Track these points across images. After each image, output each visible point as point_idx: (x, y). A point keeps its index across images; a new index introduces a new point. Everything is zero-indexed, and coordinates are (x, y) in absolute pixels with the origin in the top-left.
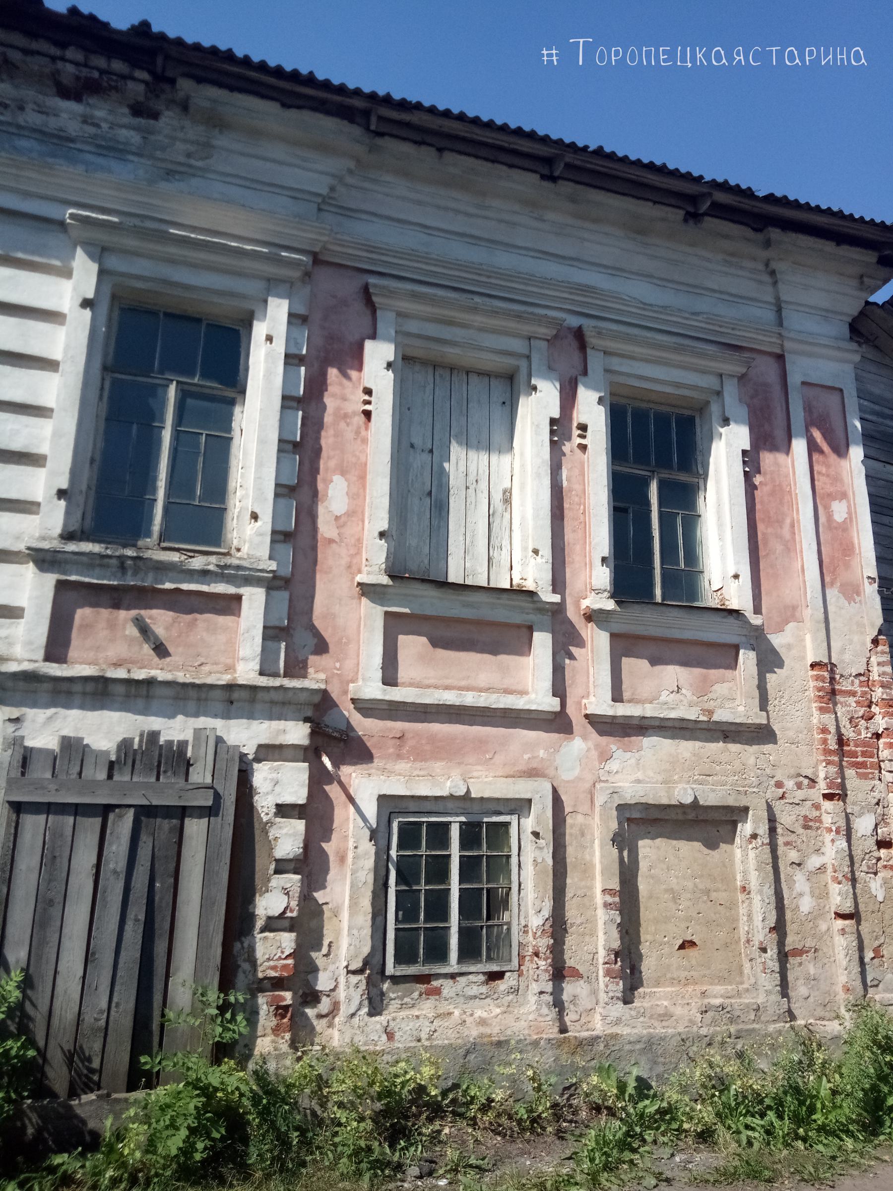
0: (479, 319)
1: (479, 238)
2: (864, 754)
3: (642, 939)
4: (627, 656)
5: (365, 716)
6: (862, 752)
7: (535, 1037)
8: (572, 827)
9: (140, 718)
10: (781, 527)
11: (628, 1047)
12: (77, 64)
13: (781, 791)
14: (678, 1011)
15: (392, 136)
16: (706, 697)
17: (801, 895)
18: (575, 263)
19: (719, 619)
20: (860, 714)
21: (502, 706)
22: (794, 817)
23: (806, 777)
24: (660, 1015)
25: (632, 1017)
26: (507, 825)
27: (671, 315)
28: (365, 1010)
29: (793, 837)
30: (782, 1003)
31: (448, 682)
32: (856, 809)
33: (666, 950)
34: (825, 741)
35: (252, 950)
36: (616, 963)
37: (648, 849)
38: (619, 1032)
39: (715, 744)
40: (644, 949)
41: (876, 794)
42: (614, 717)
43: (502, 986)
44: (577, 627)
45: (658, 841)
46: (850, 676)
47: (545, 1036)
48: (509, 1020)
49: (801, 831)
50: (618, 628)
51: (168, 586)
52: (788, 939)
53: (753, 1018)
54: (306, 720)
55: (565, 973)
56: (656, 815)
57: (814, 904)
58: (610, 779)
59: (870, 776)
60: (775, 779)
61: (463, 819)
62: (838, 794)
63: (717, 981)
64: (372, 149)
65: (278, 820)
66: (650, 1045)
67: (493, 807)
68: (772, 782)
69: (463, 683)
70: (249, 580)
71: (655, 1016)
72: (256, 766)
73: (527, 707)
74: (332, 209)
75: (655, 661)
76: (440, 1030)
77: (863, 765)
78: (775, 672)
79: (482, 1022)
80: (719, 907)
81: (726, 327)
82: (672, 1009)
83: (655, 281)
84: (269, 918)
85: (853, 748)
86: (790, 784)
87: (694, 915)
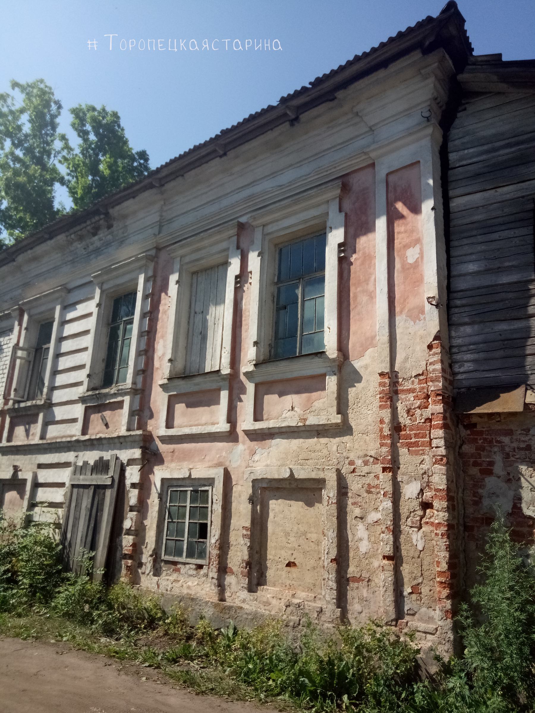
0: (206, 242)
1: (214, 200)
2: (416, 435)
3: (268, 558)
4: (267, 394)
5: (163, 443)
6: (415, 434)
7: (207, 600)
8: (235, 492)
9: (101, 452)
10: (367, 284)
11: (245, 616)
12: (90, 225)
13: (353, 467)
14: (274, 602)
15: (167, 182)
16: (309, 410)
17: (361, 540)
18: (255, 184)
19: (309, 361)
20: (417, 405)
21: (206, 432)
22: (360, 486)
23: (371, 456)
24: (264, 602)
25: (251, 600)
26: (207, 491)
27: (296, 183)
28: (152, 573)
29: (359, 499)
30: (336, 611)
31: (191, 423)
32: (405, 478)
33: (280, 566)
34: (381, 430)
35: (121, 541)
36: (246, 568)
37: (274, 506)
38: (243, 607)
39: (312, 440)
40: (269, 564)
41: (425, 467)
42: (255, 430)
43: (203, 572)
44: (244, 383)
45: (280, 500)
46: (411, 377)
47: (211, 600)
48: (199, 588)
49: (365, 495)
50: (258, 380)
51: (108, 401)
52: (349, 569)
53: (316, 617)
54: (141, 448)
55: (227, 570)
56: (276, 485)
57: (370, 547)
58: (254, 465)
59: (421, 452)
60: (349, 459)
61: (191, 489)
62: (388, 467)
63: (307, 590)
64: (162, 193)
65: (131, 489)
66: (255, 616)
67: (202, 482)
68: (347, 462)
69: (196, 423)
70: (126, 394)
71: (262, 602)
72: (127, 468)
73: (216, 431)
74: (165, 223)
75: (281, 394)
76: (174, 588)
77: (416, 444)
78: (355, 386)
79: (189, 587)
80: (312, 544)
81: (330, 169)
82: (271, 600)
83: (296, 166)
84: (127, 530)
85: (408, 432)
86: (359, 462)
87: (297, 546)
